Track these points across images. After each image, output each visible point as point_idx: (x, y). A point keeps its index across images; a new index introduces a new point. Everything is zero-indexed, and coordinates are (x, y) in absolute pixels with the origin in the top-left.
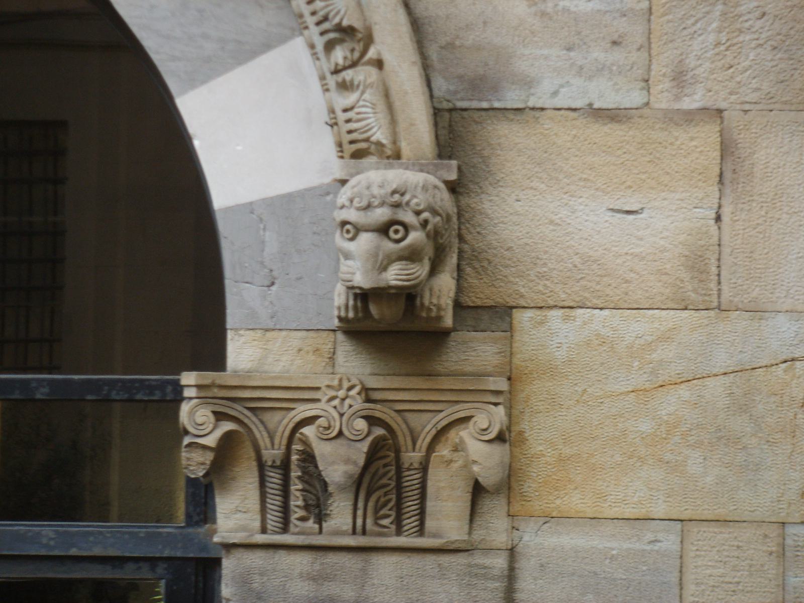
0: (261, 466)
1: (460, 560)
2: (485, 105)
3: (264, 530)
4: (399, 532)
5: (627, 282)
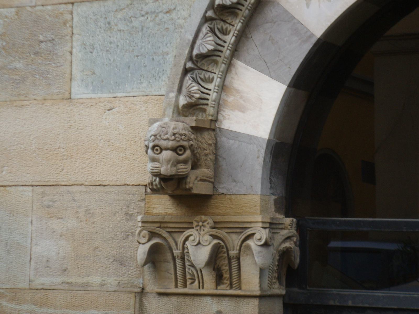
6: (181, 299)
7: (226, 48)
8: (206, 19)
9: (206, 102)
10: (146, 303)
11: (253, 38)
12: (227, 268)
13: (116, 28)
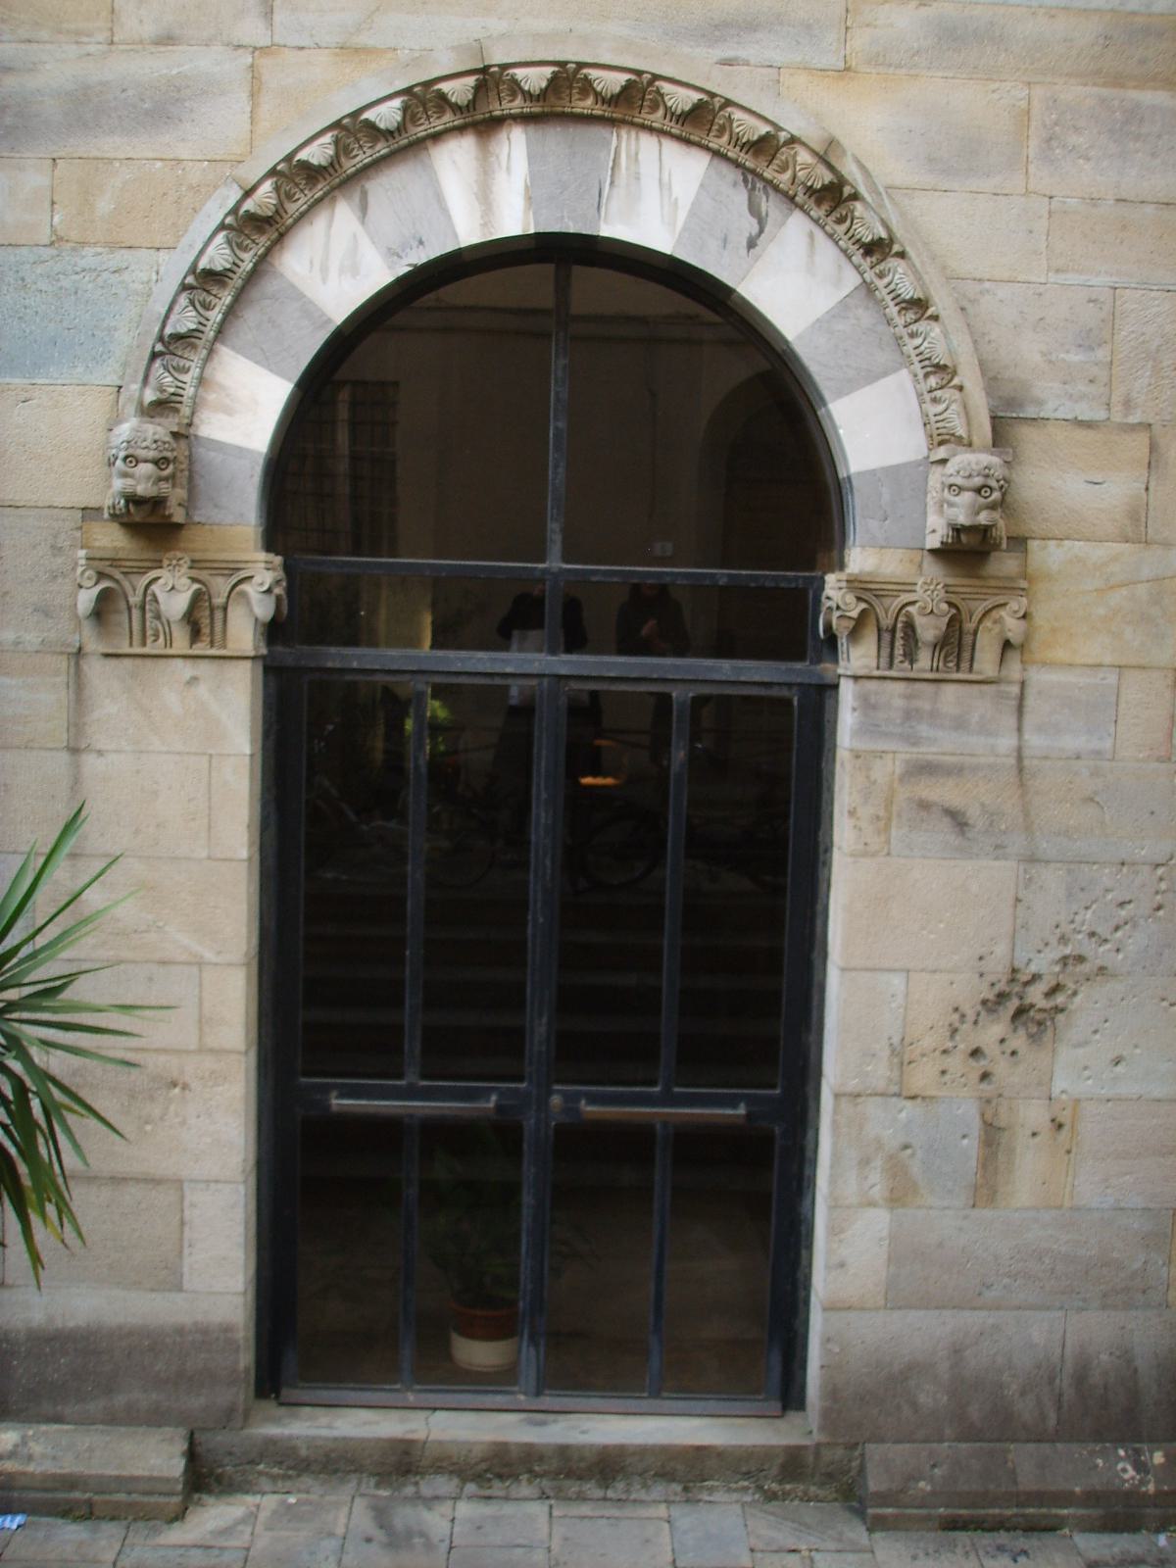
0: (879, 630)
1: (993, 687)
2: (1014, 415)
3: (878, 668)
4: (958, 669)
5: (1094, 525)
6: (138, 661)
7: (208, 328)
8: (185, 287)
9: (179, 399)
10: (85, 667)
11: (246, 317)
12: (208, 621)
13: (34, 287)
